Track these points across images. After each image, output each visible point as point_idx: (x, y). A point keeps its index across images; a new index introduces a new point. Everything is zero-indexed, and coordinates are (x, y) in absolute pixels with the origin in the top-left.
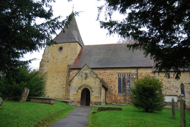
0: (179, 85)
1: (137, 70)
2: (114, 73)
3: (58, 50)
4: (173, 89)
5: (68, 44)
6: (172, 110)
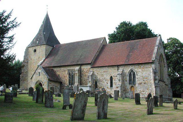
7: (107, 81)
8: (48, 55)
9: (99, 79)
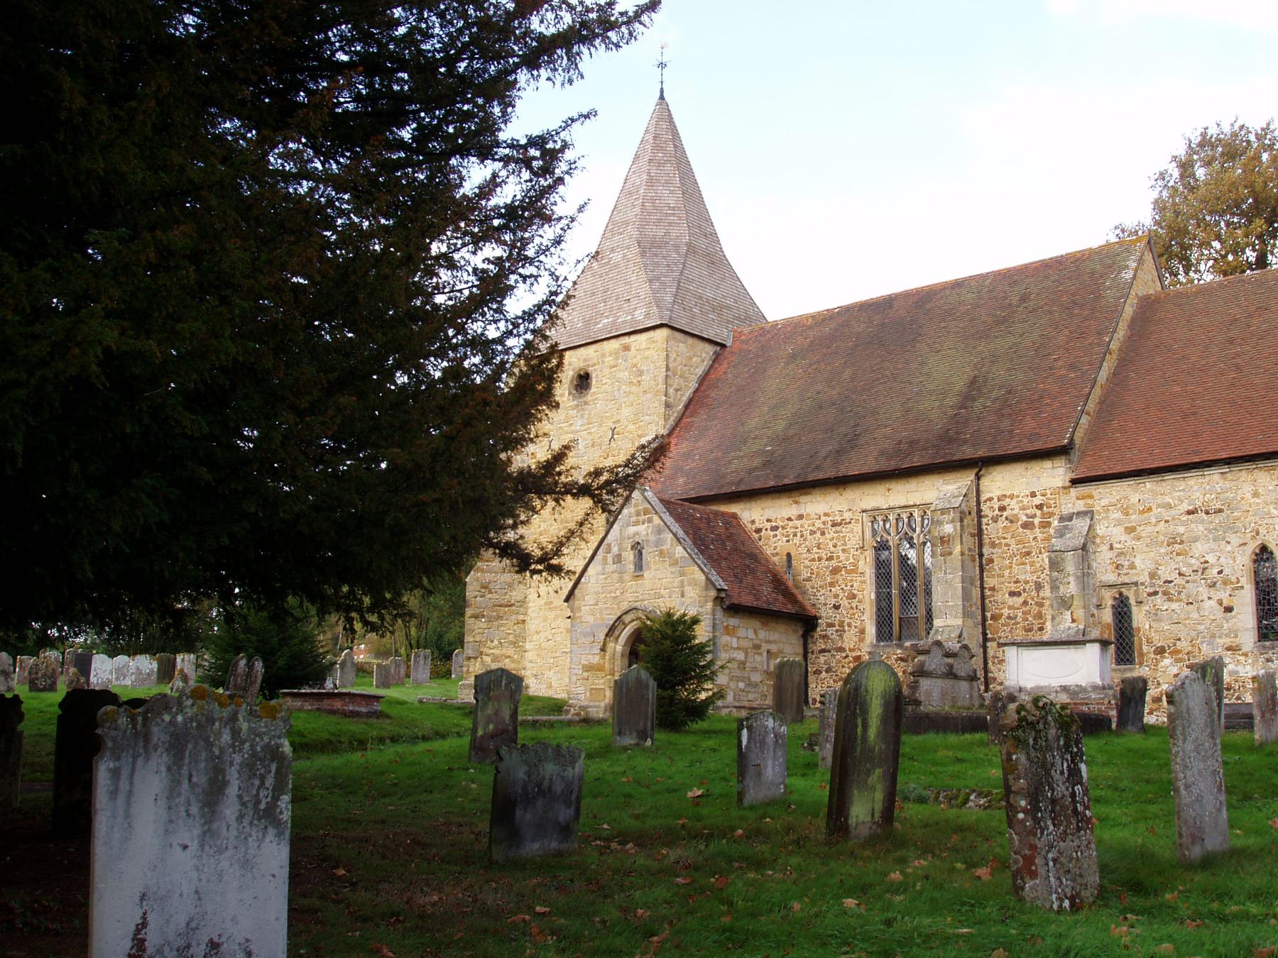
0: (1244, 559)
1: (978, 477)
2: (847, 516)
3: (570, 393)
4: (1203, 591)
5: (614, 344)
6: (898, 751)
7: (1223, 595)
8: (687, 407)
9: (1144, 578)
